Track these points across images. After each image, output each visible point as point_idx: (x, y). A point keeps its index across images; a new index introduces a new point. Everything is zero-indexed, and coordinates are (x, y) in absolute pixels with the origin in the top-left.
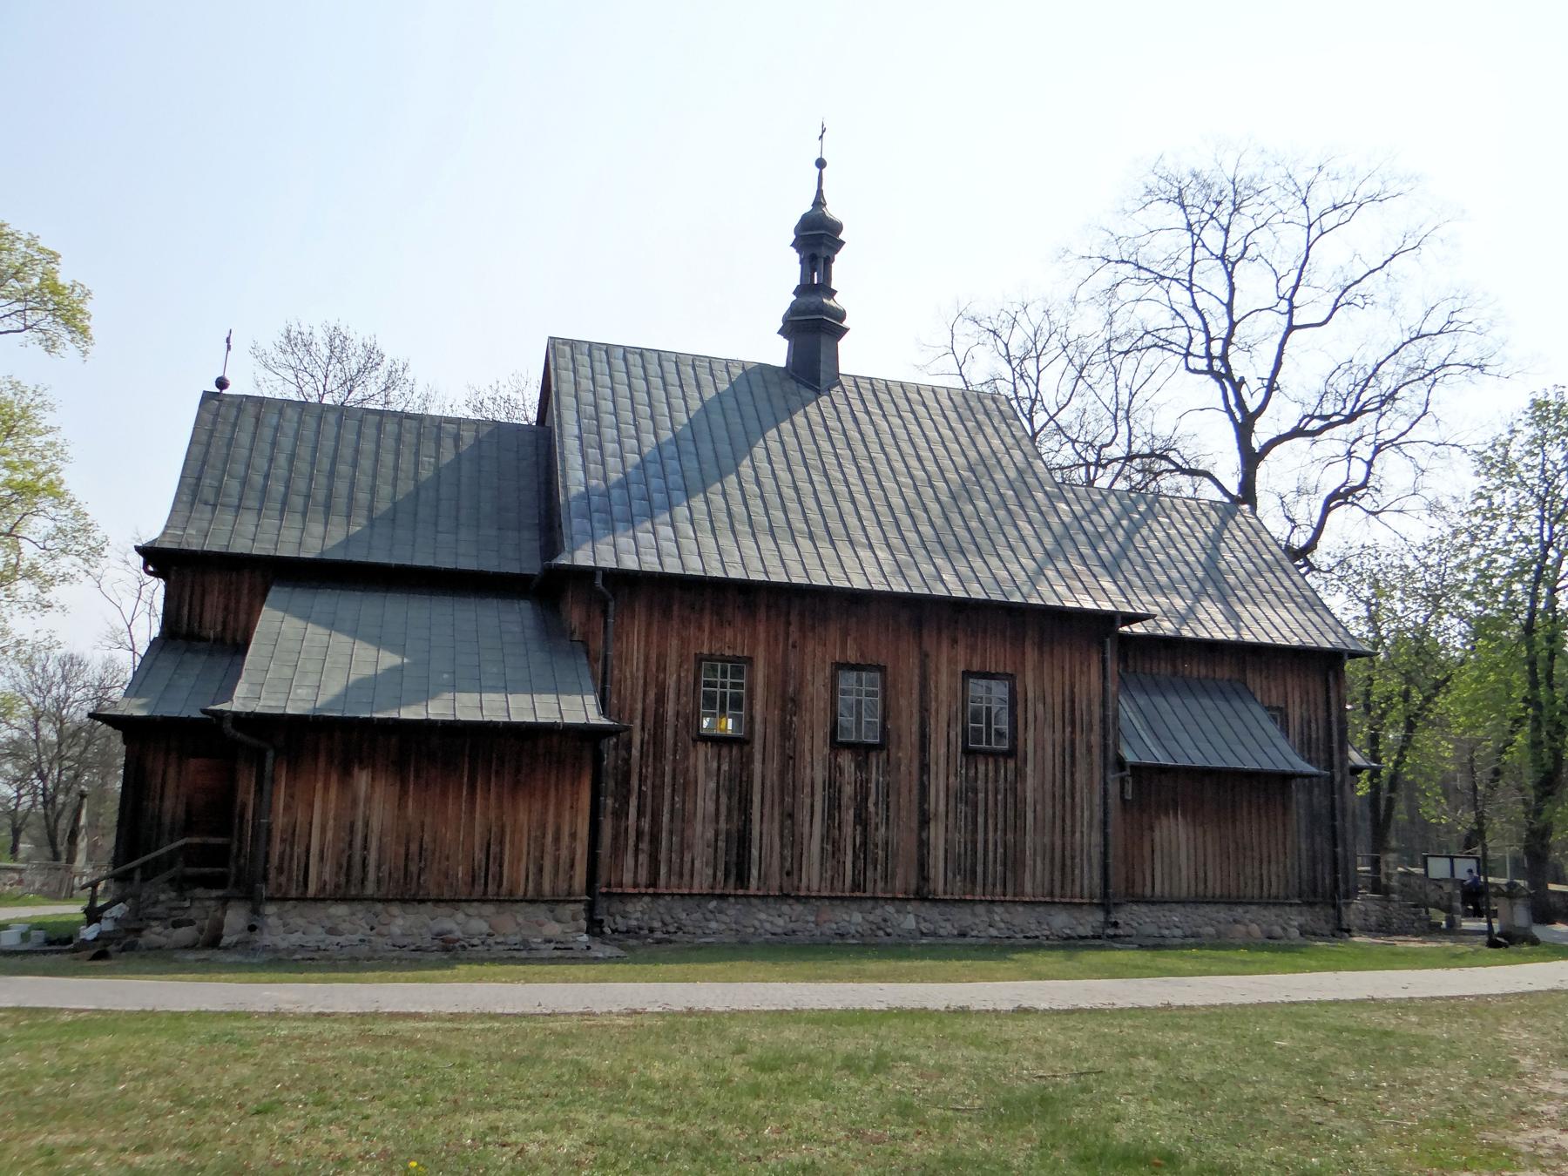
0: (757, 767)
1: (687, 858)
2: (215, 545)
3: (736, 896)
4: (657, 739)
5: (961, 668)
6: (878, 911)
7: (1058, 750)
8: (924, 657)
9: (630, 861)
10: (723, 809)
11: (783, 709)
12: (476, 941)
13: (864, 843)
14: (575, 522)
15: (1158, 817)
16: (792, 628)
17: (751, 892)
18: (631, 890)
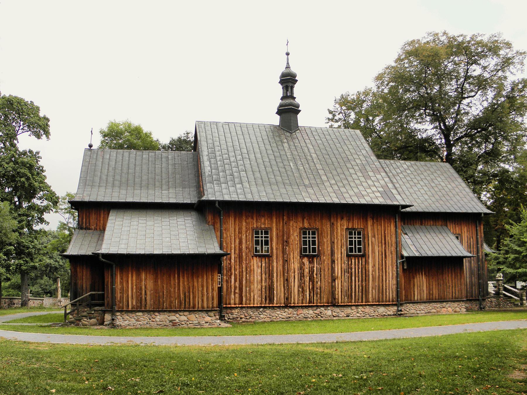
0: (275, 264)
1: (252, 295)
2: (93, 199)
3: (269, 307)
4: (240, 257)
5: (345, 227)
6: (318, 310)
7: (380, 253)
9: (233, 296)
10: (263, 279)
11: (283, 245)
12: (183, 323)
13: (313, 288)
14: (208, 184)
15: (416, 274)
16: (285, 217)
17: (275, 305)
18: (233, 306)
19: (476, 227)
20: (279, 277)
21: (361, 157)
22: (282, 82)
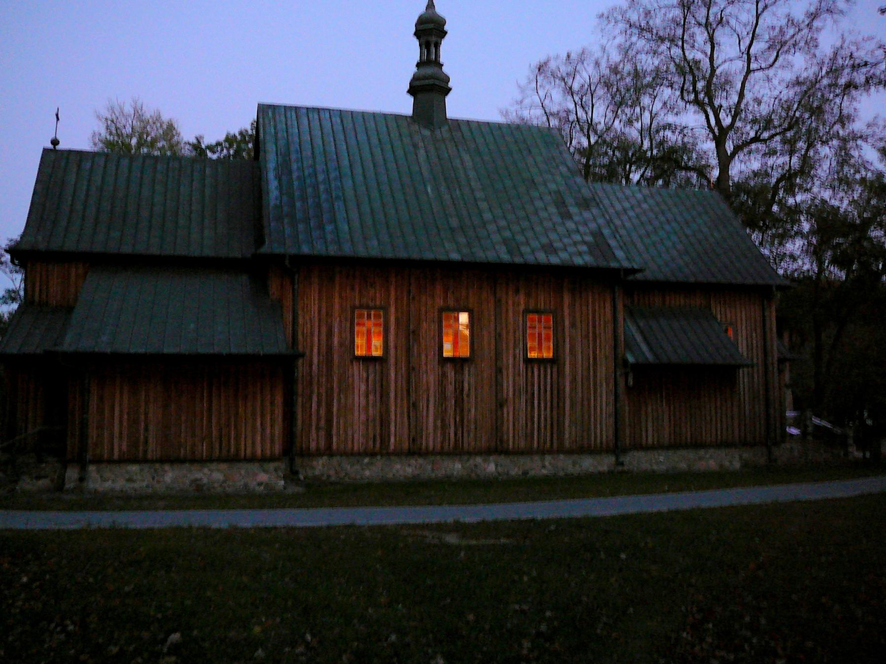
4: (329, 362)
5: (522, 307)
8: (498, 302)
19: (763, 310)
20: (399, 401)
21: (559, 179)
22: (418, 34)
